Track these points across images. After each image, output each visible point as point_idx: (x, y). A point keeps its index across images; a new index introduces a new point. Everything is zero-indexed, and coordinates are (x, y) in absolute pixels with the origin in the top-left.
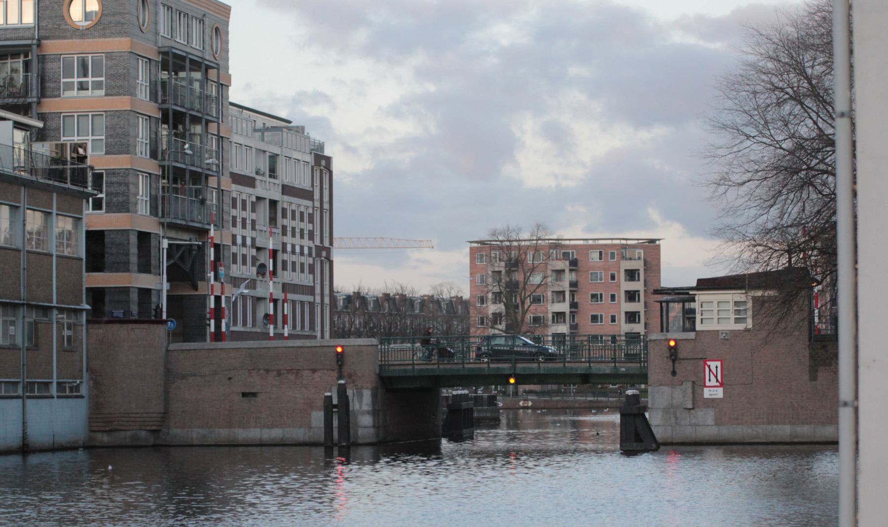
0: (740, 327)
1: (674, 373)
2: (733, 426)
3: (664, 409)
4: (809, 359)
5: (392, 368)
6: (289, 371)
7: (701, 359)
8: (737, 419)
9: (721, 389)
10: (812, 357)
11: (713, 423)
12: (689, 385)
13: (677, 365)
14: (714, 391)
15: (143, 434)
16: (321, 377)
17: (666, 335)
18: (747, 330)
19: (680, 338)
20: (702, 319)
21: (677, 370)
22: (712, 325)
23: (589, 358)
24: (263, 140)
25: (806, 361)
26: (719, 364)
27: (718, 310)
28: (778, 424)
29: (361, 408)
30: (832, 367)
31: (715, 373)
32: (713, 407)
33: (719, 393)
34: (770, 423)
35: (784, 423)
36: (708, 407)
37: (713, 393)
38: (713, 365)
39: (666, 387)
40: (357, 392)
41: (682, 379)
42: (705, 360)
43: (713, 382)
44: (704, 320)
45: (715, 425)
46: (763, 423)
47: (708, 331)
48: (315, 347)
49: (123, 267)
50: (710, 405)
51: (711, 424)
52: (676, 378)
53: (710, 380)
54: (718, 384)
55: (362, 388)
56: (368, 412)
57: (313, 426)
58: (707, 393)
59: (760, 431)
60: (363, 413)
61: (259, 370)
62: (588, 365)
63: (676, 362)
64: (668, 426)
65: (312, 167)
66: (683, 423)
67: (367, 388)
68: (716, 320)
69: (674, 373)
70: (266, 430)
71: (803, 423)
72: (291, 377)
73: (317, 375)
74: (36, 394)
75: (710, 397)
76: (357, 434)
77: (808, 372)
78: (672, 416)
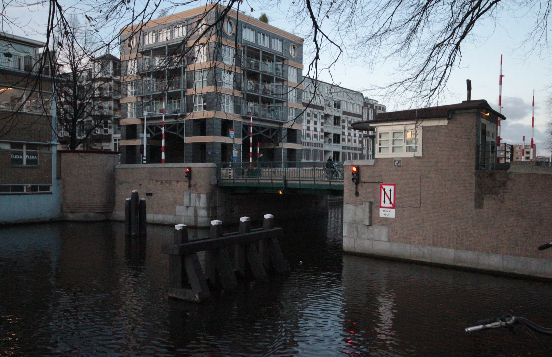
0: (411, 155)
1: (357, 194)
2: (402, 244)
3: (349, 223)
4: (476, 186)
5: (224, 181)
6: (166, 182)
7: (378, 183)
8: (406, 238)
9: (394, 210)
10: (479, 185)
11: (386, 240)
12: (366, 206)
13: (360, 188)
14: (387, 211)
15: (92, 214)
16: (181, 186)
17: (352, 162)
18: (418, 158)
19: (362, 165)
20: (393, 148)
21: (360, 192)
22: (388, 153)
23: (300, 177)
24: (337, 95)
25: (473, 188)
26: (392, 187)
27: (393, 140)
28: (442, 246)
29: (199, 205)
30: (499, 196)
31: (386, 196)
32: (387, 225)
33: (392, 214)
34: (434, 244)
35: (449, 247)
36: (383, 225)
37: (387, 213)
38: (388, 188)
39: (351, 205)
40: (198, 195)
41: (364, 200)
42: (382, 184)
43: (387, 204)
44: (382, 150)
45: (388, 241)
46: (429, 245)
47: (385, 158)
48: (178, 167)
49: (213, 134)
50: (384, 223)
51: (385, 240)
52: (359, 198)
53: (384, 202)
54: (391, 206)
55: (200, 193)
56: (204, 208)
57: (177, 214)
58: (382, 213)
59: (426, 252)
60: (201, 208)
61: (153, 180)
62: (329, 183)
63: (359, 185)
64: (352, 237)
65: (363, 107)
66: (363, 237)
67: (203, 193)
68: (391, 149)
69: (357, 194)
70: (156, 215)
71: (467, 249)
72: (167, 185)
73: (179, 184)
74: (39, 192)
75: (384, 216)
76: (197, 221)
77: (473, 199)
78: (354, 230)
